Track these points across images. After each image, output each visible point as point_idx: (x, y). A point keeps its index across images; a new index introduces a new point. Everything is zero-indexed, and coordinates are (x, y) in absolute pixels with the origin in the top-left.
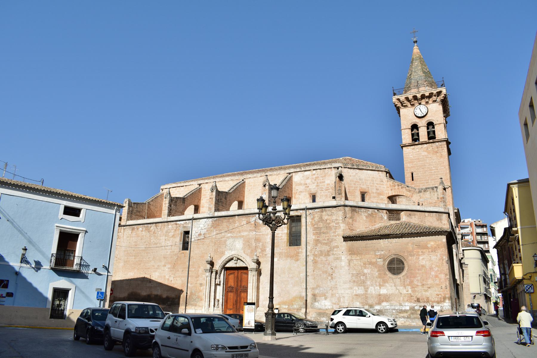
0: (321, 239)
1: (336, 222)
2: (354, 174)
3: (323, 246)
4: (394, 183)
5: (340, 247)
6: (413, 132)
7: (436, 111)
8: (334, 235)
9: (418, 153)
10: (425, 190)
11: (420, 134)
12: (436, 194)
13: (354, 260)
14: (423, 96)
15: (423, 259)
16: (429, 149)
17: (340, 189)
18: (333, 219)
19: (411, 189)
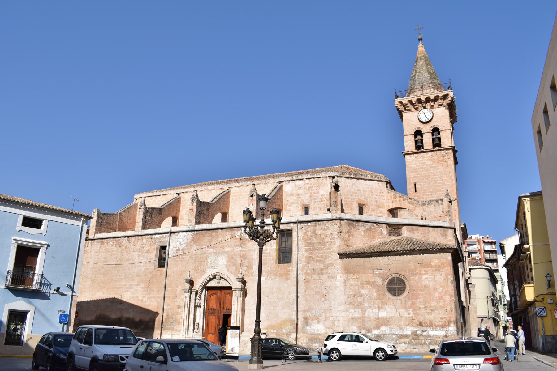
0: (313, 255)
1: (330, 237)
3: (316, 264)
8: (328, 252)
9: (422, 161)
10: (429, 202)
11: (424, 141)
12: (441, 207)
13: (351, 280)
14: (428, 99)
15: (426, 278)
16: (434, 158)
17: (336, 200)
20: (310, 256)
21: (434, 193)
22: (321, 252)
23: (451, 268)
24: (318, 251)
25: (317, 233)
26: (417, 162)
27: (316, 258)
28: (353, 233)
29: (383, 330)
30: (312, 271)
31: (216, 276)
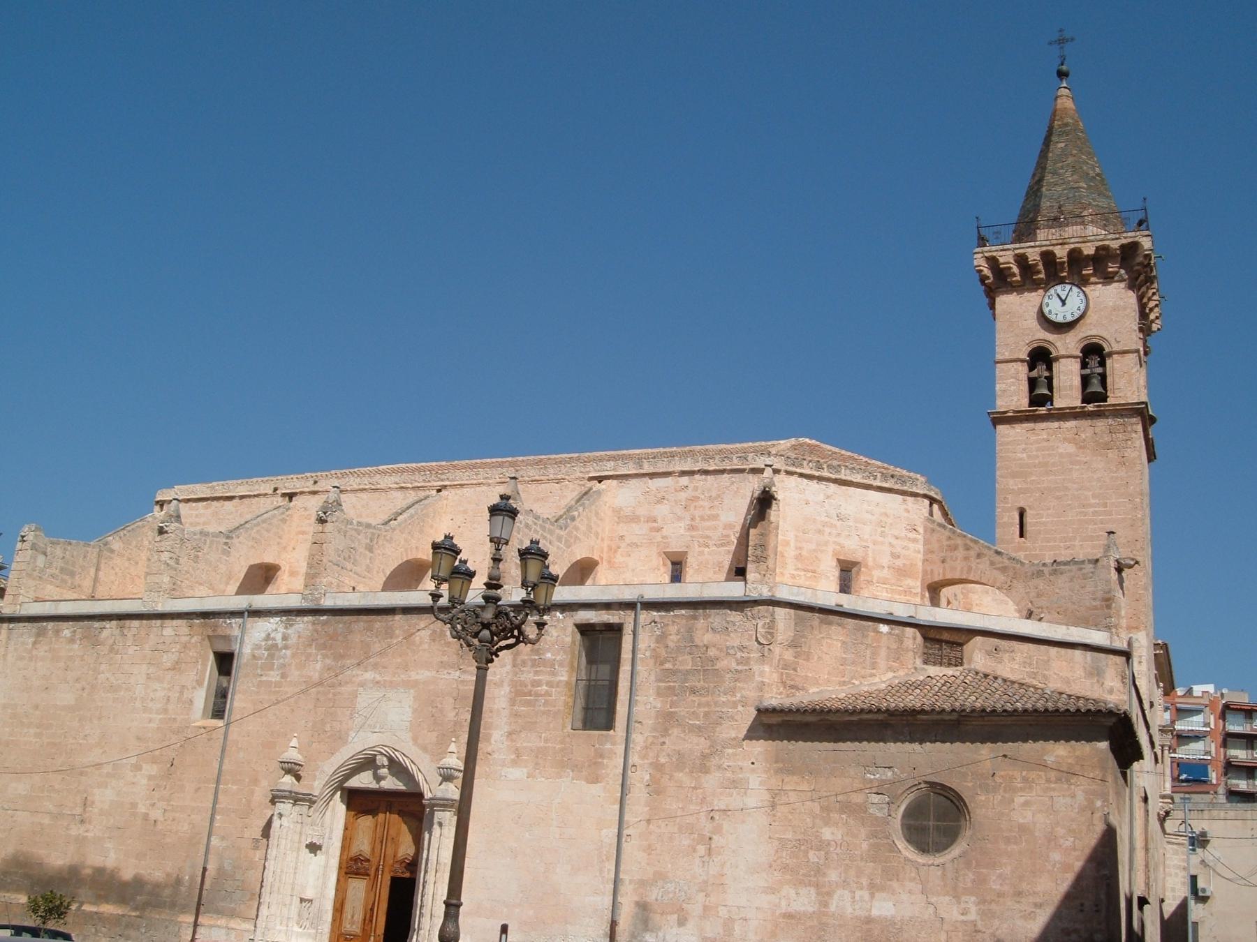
0: (681, 711)
3: (687, 738)
6: (1034, 374)
9: (1045, 444)
13: (790, 793)
15: (1026, 804)
21: (1077, 543)
26: (1031, 444)
27: (690, 719)
28: (810, 647)
30: (674, 759)
31: (376, 755)
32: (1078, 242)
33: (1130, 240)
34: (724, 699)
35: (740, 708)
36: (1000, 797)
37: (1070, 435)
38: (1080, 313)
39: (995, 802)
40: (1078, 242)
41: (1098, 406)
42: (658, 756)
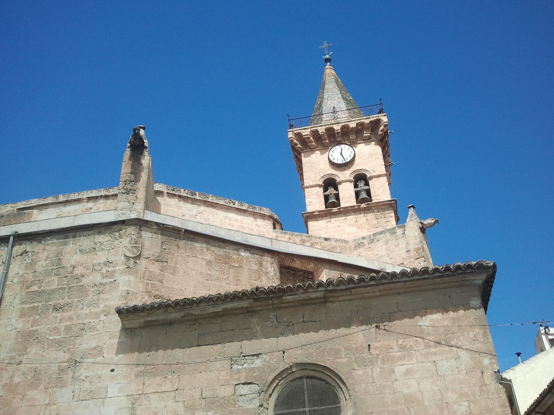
0: (42, 328)
1: (104, 270)
2: (195, 212)
3: (45, 354)
4: (293, 237)
5: (105, 351)
6: (327, 193)
7: (370, 155)
8: (91, 313)
9: (339, 228)
10: (372, 238)
11: (341, 196)
13: (152, 396)
14: (345, 130)
15: (409, 372)
16: (360, 222)
18: (95, 262)
19: (334, 244)
20: (33, 331)
22: (66, 314)
23: (485, 333)
24: (58, 315)
25: (64, 263)
26: (330, 229)
27: (50, 335)
28: (176, 263)
29: (84, 236)
30: (29, 378)
32: (346, 122)
33: (375, 118)
34: (86, 311)
35: (102, 318)
36: (378, 369)
37: (352, 222)
38: (351, 158)
39: (375, 375)
40: (346, 122)
41: (367, 204)
42: (12, 377)
